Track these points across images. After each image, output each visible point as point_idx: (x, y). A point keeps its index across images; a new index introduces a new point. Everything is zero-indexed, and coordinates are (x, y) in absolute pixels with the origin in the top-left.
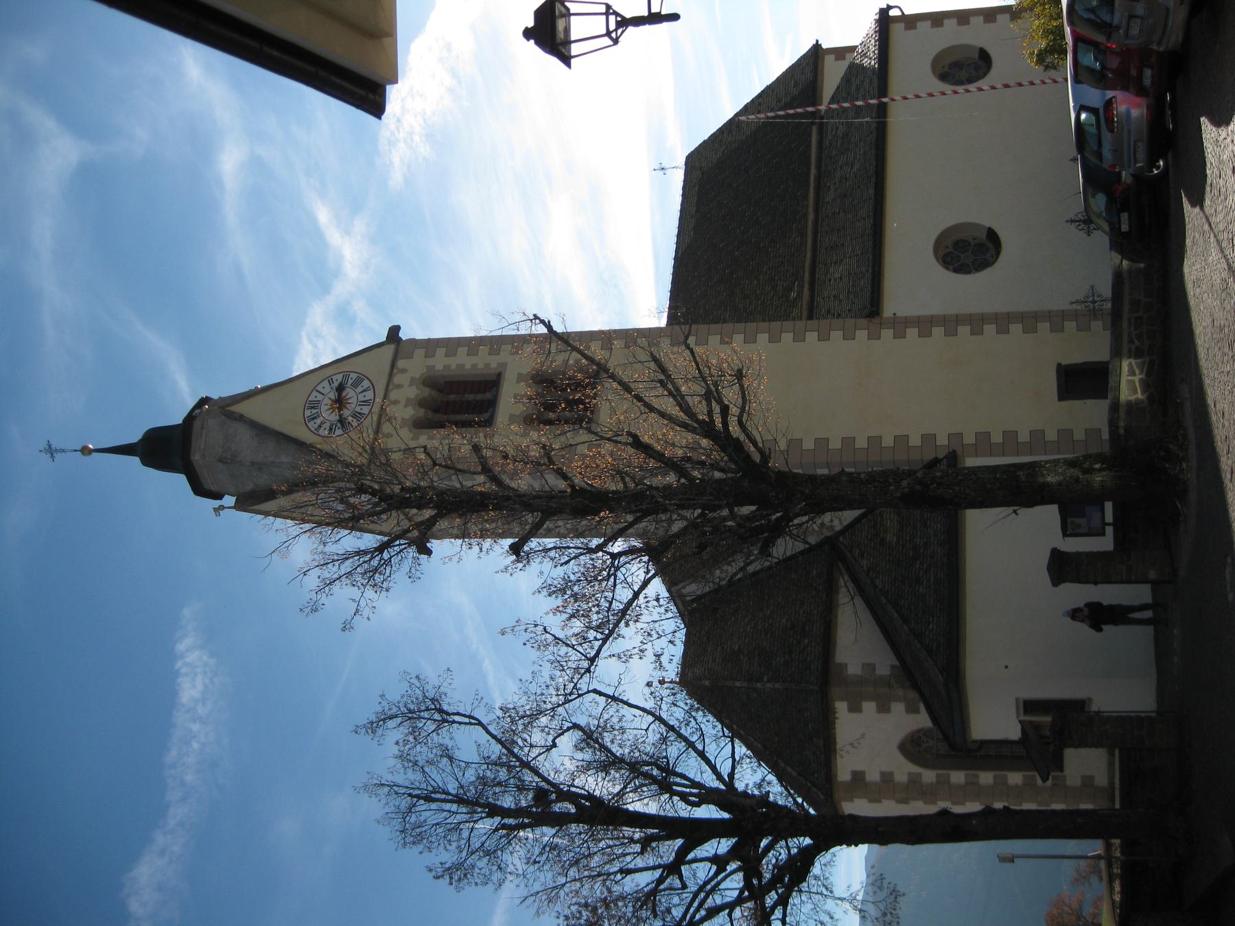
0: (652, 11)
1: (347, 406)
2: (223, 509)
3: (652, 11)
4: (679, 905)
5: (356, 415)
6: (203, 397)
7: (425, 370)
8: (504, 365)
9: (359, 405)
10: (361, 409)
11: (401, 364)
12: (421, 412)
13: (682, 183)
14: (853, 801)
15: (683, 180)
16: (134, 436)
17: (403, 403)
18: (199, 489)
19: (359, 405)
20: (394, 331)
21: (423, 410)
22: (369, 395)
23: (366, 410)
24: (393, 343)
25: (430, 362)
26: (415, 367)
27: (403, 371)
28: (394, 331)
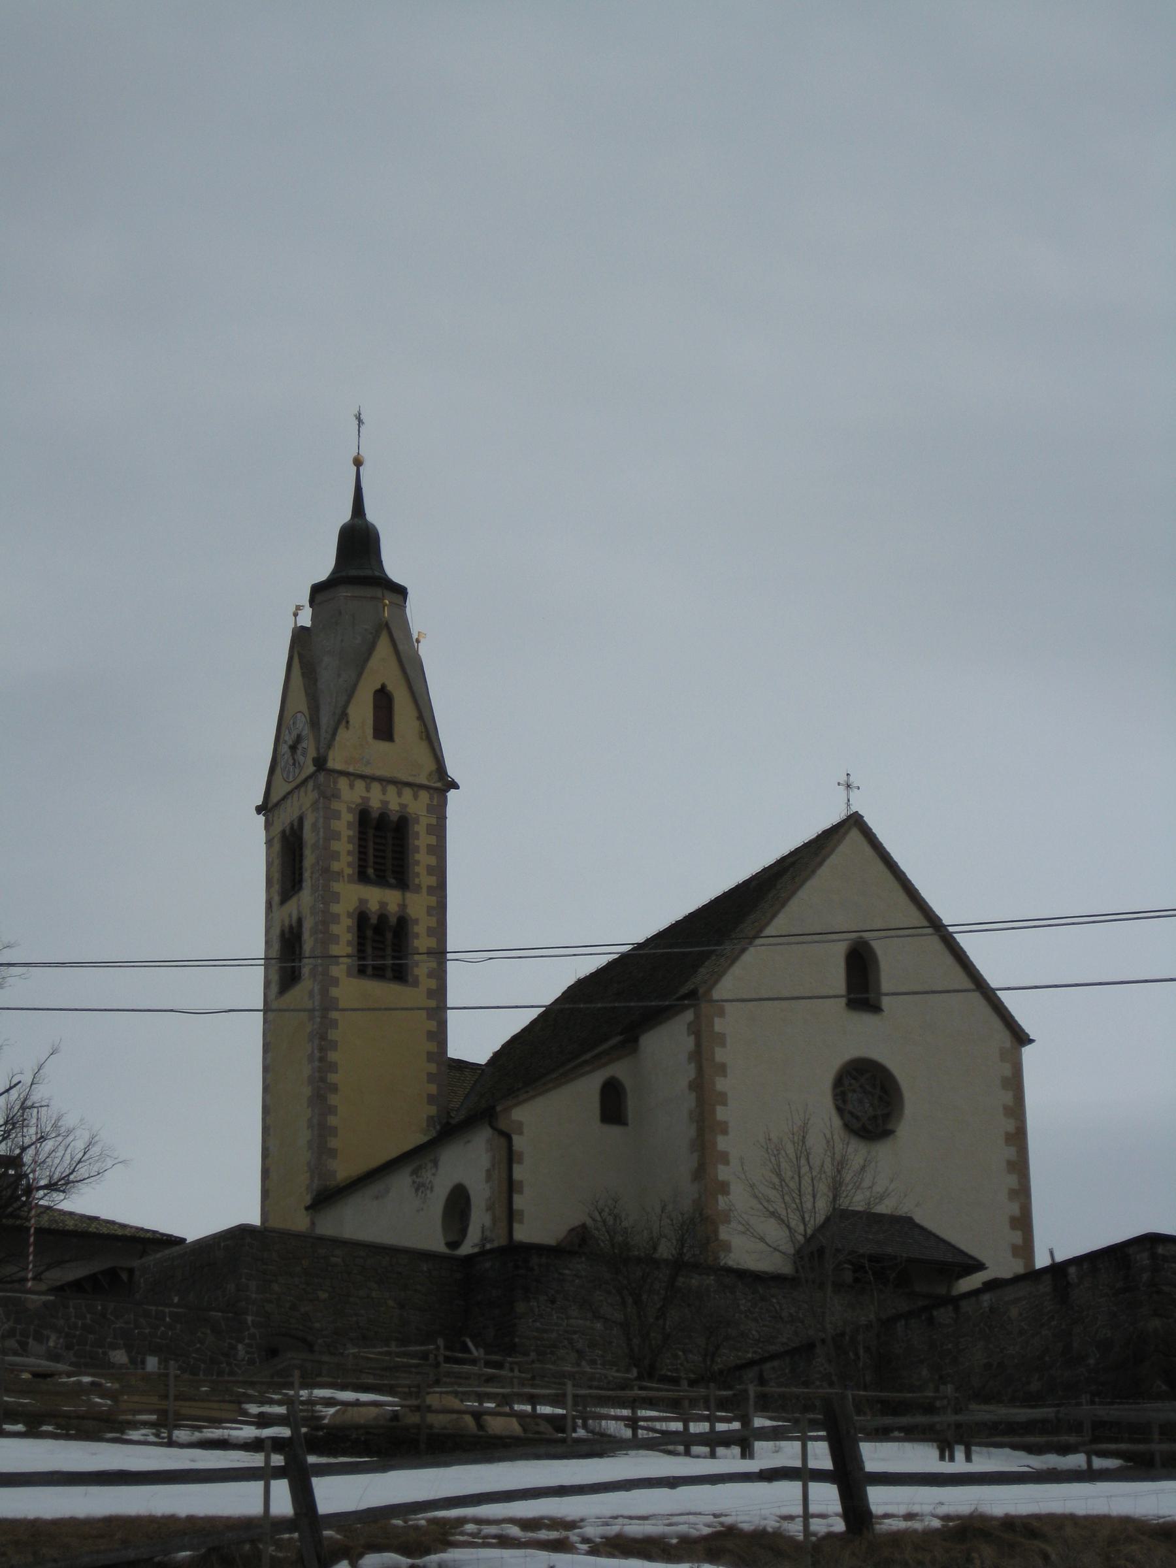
18: (317, 590)
20: (455, 785)
26: (417, 806)
28: (455, 785)
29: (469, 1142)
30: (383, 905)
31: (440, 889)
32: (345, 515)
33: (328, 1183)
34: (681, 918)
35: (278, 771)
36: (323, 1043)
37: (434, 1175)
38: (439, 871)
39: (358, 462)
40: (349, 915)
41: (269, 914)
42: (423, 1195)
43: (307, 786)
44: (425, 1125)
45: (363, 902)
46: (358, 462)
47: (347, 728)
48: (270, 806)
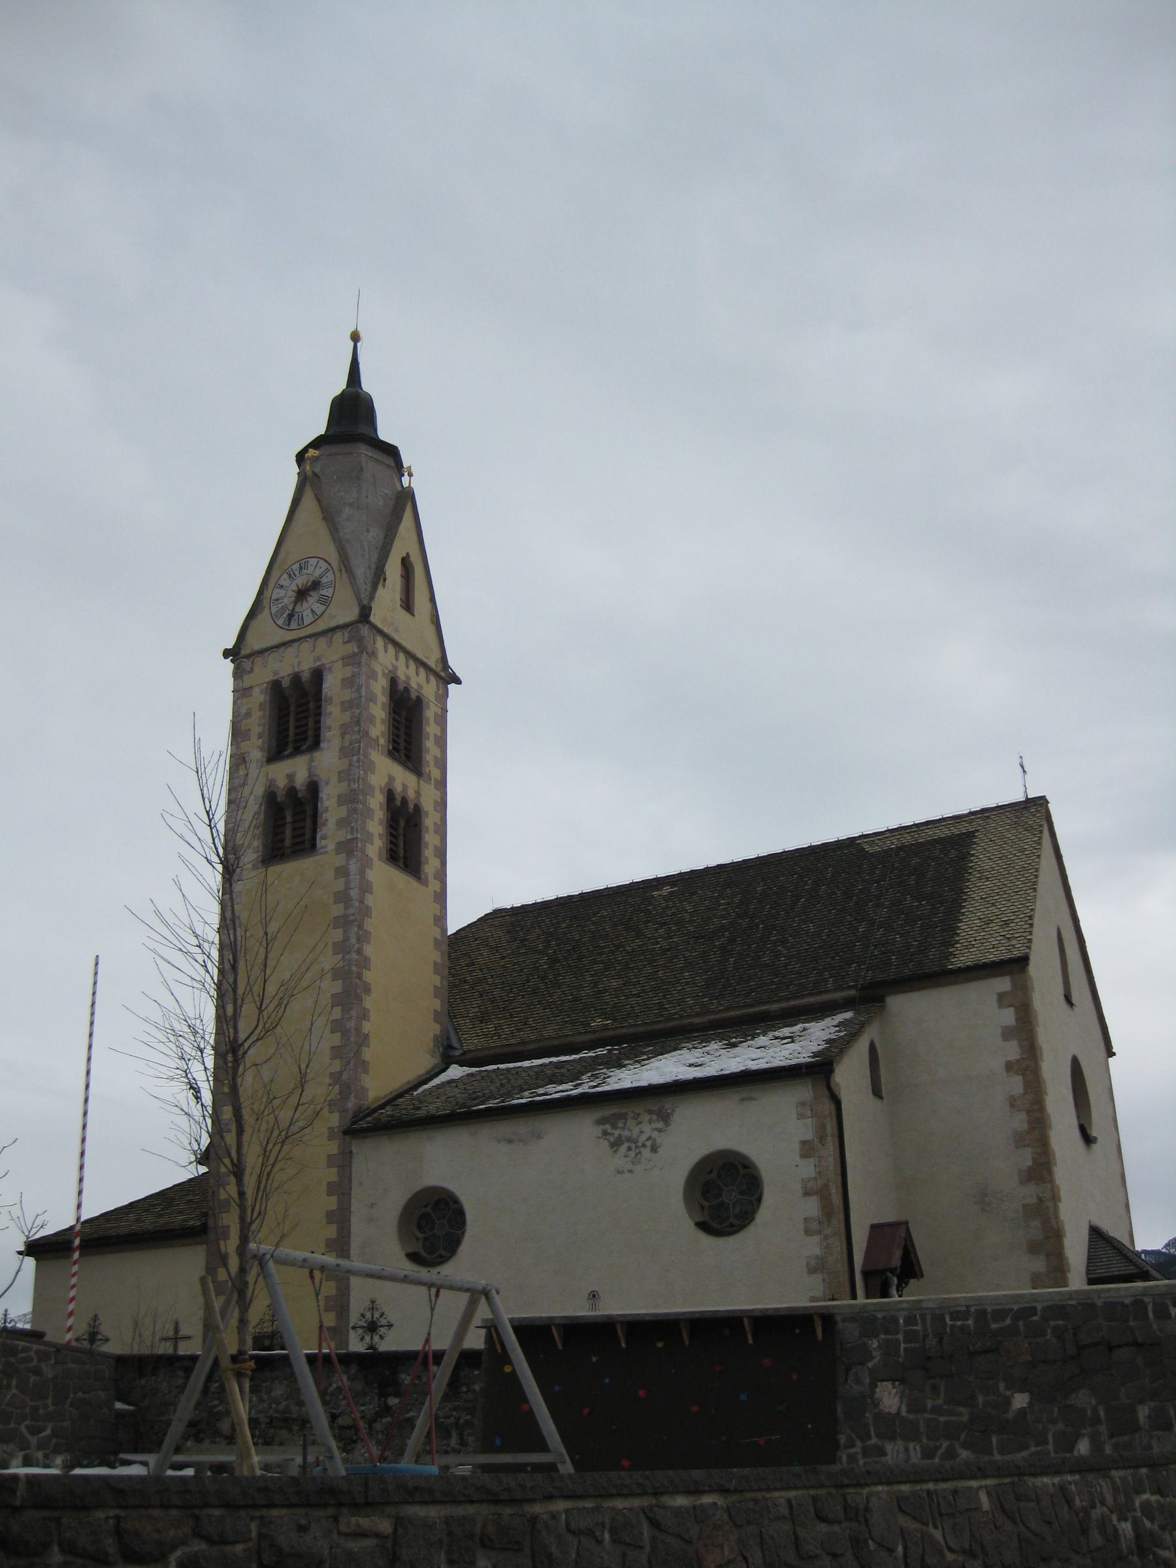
26: (426, 687)
28: (458, 681)
29: (751, 1099)
30: (405, 787)
31: (442, 784)
32: (339, 384)
33: (362, 1102)
34: (702, 868)
35: (264, 616)
36: (360, 932)
37: (660, 1131)
38: (442, 764)
39: (355, 337)
40: (381, 791)
41: (237, 770)
42: (632, 1154)
43: (317, 639)
44: (432, 1045)
45: (271, 783)
46: (355, 337)
47: (384, 587)
48: (243, 652)
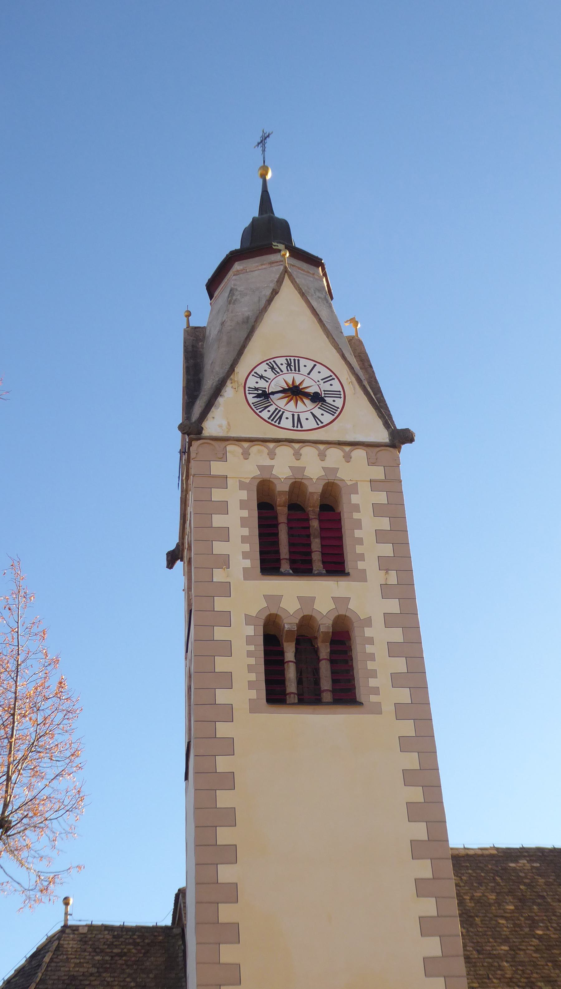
0: (387, 440)
1: (292, 401)
2: (186, 316)
3: (387, 440)
4: (18, 798)
5: (278, 417)
6: (322, 260)
7: (349, 483)
8: (362, 577)
9: (293, 415)
10: (287, 418)
11: (360, 454)
12: (283, 487)
13: (518, 846)
14: (153, 926)
15: (526, 845)
16: (279, 212)
17: (297, 464)
19: (293, 415)
21: (287, 489)
22: (310, 424)
23: (286, 423)
24: (390, 440)
25: (364, 488)
27: (348, 458)
